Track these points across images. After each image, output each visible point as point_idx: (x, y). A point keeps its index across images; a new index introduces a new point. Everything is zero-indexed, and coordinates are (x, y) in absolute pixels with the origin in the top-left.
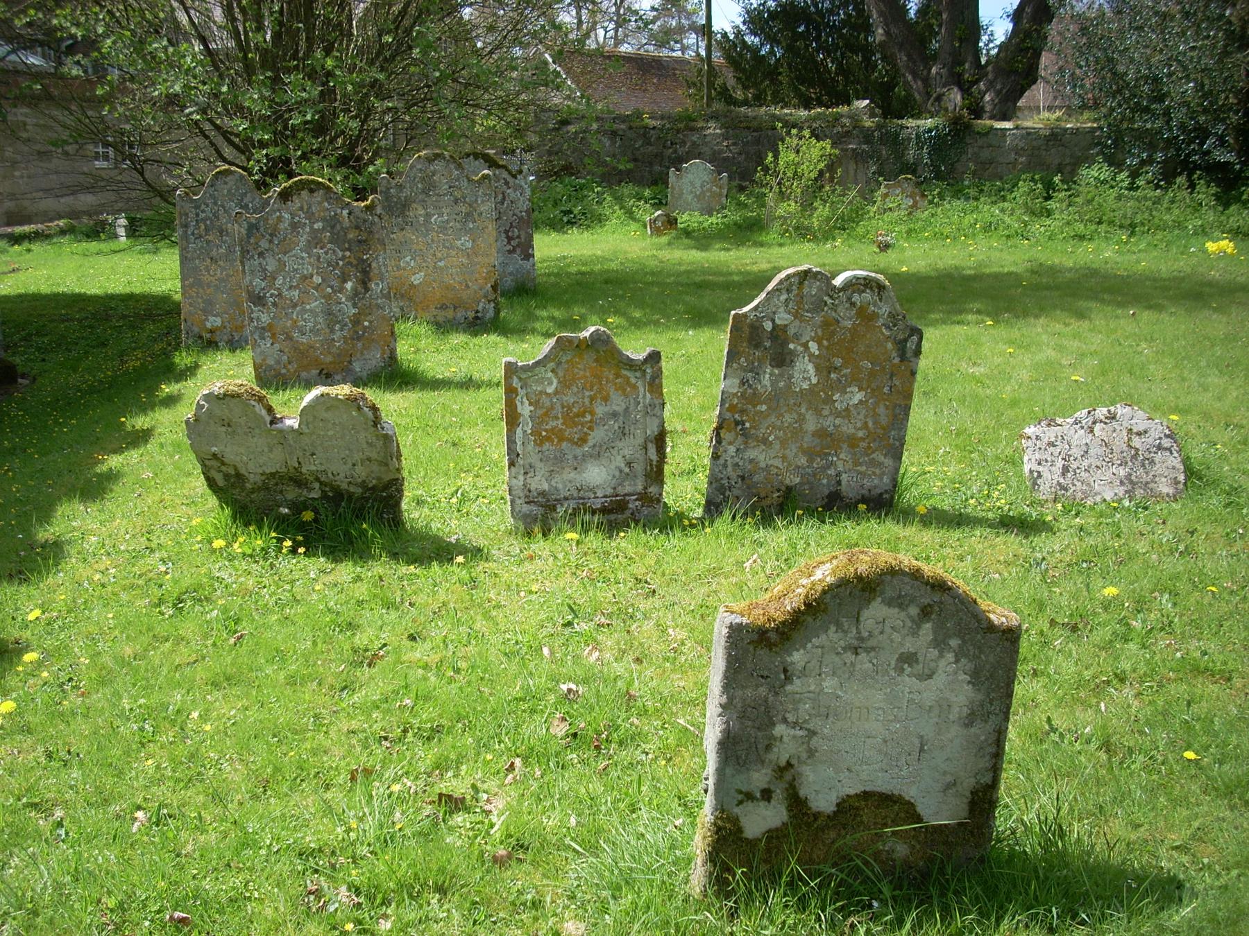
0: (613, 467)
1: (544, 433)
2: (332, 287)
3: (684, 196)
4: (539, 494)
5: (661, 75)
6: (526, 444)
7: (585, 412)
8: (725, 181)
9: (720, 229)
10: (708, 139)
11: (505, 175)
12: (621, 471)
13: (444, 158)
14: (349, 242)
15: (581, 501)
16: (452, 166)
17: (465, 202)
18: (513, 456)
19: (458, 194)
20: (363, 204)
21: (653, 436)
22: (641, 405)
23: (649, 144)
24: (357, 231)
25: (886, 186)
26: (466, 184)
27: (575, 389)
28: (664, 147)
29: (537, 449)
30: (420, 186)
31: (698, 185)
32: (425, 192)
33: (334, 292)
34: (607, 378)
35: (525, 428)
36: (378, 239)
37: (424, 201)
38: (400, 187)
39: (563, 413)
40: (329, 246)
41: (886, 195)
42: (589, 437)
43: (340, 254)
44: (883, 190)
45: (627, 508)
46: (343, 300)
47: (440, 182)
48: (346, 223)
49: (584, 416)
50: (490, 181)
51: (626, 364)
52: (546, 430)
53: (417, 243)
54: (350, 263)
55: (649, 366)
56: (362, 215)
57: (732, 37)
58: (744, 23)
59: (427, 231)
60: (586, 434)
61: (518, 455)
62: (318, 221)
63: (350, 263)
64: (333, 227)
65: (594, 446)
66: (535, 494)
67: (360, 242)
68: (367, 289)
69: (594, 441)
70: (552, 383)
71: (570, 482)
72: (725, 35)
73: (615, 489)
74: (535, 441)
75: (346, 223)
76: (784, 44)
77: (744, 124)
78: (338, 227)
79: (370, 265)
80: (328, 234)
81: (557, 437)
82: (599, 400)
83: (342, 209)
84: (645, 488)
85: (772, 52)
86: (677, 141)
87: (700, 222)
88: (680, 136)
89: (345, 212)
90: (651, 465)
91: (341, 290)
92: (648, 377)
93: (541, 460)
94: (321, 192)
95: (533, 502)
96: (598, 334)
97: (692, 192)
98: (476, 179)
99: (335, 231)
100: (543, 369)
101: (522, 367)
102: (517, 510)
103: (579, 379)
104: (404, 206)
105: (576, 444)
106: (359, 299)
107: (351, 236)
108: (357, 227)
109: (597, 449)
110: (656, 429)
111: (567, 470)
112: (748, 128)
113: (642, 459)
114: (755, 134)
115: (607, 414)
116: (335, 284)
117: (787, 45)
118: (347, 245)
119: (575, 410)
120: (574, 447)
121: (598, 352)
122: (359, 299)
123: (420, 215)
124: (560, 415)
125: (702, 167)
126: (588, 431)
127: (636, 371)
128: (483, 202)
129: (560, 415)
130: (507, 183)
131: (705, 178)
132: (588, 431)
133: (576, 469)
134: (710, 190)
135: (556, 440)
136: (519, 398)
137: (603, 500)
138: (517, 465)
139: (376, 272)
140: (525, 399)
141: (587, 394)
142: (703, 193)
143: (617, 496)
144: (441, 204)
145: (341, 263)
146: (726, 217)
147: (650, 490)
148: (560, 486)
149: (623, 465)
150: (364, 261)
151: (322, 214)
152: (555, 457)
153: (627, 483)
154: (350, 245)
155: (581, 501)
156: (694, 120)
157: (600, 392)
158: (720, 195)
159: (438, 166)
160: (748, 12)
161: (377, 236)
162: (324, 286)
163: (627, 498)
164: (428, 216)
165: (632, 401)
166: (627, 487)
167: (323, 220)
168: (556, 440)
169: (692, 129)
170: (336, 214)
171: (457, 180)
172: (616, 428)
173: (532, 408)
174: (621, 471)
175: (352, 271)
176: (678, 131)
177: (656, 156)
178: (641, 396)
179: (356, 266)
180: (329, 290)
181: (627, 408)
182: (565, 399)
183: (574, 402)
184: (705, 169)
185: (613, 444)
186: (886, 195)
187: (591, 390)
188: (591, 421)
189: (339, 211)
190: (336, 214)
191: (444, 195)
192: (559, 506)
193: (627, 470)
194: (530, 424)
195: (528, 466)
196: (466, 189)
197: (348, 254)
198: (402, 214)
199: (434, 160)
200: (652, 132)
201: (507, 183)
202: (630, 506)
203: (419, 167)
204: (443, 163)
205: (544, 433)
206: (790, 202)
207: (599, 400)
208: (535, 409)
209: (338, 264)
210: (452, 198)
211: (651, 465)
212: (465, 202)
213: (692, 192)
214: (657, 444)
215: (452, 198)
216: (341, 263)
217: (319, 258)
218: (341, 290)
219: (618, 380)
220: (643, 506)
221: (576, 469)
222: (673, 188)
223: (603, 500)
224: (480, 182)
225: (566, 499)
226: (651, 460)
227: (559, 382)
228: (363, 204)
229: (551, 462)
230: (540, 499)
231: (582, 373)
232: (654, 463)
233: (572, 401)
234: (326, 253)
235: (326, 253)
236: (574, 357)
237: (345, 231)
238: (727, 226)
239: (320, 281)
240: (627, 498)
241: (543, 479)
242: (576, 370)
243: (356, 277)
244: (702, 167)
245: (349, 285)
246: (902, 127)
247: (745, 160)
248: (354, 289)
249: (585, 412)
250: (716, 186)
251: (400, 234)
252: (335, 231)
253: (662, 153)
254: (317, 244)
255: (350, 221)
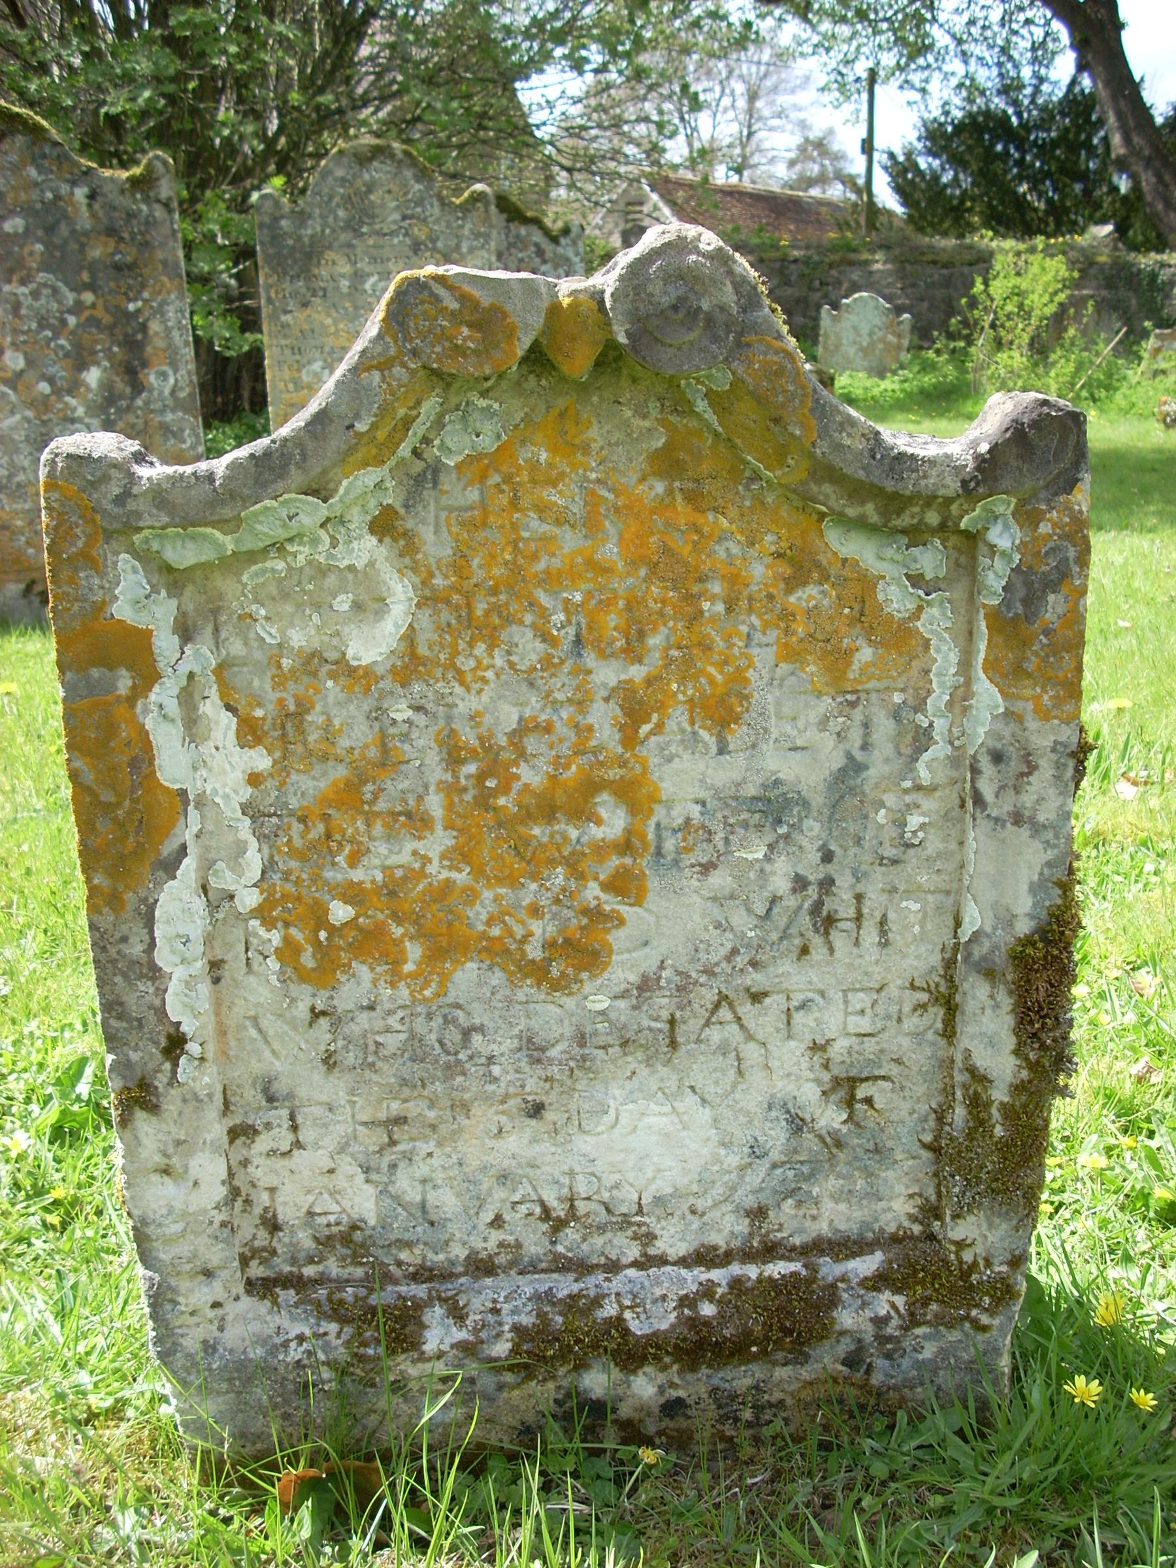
0: (752, 1098)
1: (340, 912)
2: (51, 380)
3: (843, 348)
4: (326, 1242)
5: (802, 221)
6: (235, 967)
7: (591, 787)
8: (906, 327)
9: (898, 399)
10: (876, 277)
11: (537, 236)
12: (798, 1124)
13: (392, 156)
14: (92, 267)
15: (565, 1285)
16: (409, 174)
17: (434, 249)
18: (143, 1055)
19: (420, 233)
20: (124, 175)
21: (1004, 939)
22: (939, 750)
23: (788, 283)
24: (112, 243)
25: (1157, 336)
26: (436, 211)
27: (530, 649)
28: (810, 289)
29: (305, 998)
30: (341, 213)
31: (865, 331)
32: (352, 226)
33: (57, 392)
34: (734, 580)
35: (224, 880)
36: (165, 263)
37: (350, 245)
38: (302, 217)
39: (451, 790)
40: (42, 277)
41: (1157, 351)
42: (618, 938)
43: (70, 298)
44: (1151, 343)
45: (822, 1330)
46: (81, 411)
47: (383, 206)
48: (84, 219)
49: (583, 814)
50: (487, 205)
51: (858, 491)
52: (352, 894)
53: (336, 334)
54: (94, 322)
55: (1004, 505)
56: (125, 202)
57: (901, 159)
58: (919, 139)
59: (356, 308)
60: (596, 915)
61: (175, 1044)
62: (12, 213)
63: (94, 322)
64: (51, 229)
65: (646, 986)
66: (305, 1240)
67: (118, 267)
68: (138, 387)
69: (647, 960)
70: (381, 604)
71: (504, 1178)
72: (892, 156)
73: (758, 1214)
74: (288, 952)
75: (84, 219)
76: (975, 167)
77: (929, 257)
78: (64, 229)
79: (144, 328)
80: (39, 247)
81: (421, 934)
82: (678, 718)
83: (74, 183)
84: (931, 1211)
85: (956, 181)
86: (830, 280)
87: (866, 389)
88: (834, 272)
89: (80, 193)
90: (977, 1104)
91: (74, 387)
92: (995, 577)
93: (330, 1062)
94: (20, 140)
95: (295, 1282)
96: (680, 275)
97: (855, 343)
98: (458, 201)
99: (57, 240)
100: (311, 512)
101: (160, 495)
102: (191, 1343)
103: (549, 580)
104: (309, 256)
105: (538, 972)
106: (120, 411)
107: (96, 253)
108: (111, 232)
109: (663, 1003)
110: (1023, 905)
111: (485, 1117)
112: (934, 263)
113: (920, 1057)
114: (944, 271)
115: (731, 799)
116: (60, 371)
117: (980, 170)
118: (85, 277)
119: (530, 776)
120: (527, 990)
121: (681, 405)
122: (120, 411)
123: (343, 276)
124: (435, 804)
125: (872, 304)
126: (610, 903)
127: (916, 536)
128: (471, 250)
129: (435, 804)
130: (540, 253)
131: (877, 321)
132: (610, 903)
133: (536, 1110)
134: (882, 340)
135: (414, 952)
136: (164, 694)
137: (694, 1277)
138: (171, 1103)
139: (161, 344)
140: (211, 708)
141: (607, 674)
142: (872, 344)
143: (770, 1251)
144: (386, 252)
145: (72, 320)
146: (905, 381)
147: (959, 1231)
148: (446, 1201)
149: (809, 1093)
150: (130, 316)
151: (23, 196)
152: (415, 1050)
153: (825, 1186)
154: (93, 276)
155: (565, 1285)
156: (855, 251)
157: (686, 669)
158: (899, 348)
159: (378, 172)
160: (925, 126)
161: (160, 255)
162: (30, 376)
163: (830, 1269)
164: (358, 277)
165: (884, 727)
166: (828, 1205)
167: (27, 210)
168: (414, 952)
169: (851, 263)
170: (58, 198)
171: (420, 202)
172: (781, 884)
173: (261, 760)
174: (798, 1124)
175: (102, 342)
176: (831, 266)
177: (798, 301)
178: (939, 698)
179: (111, 329)
180: (44, 387)
181: (853, 768)
182: (466, 703)
183: (525, 728)
184: (877, 308)
185: (755, 980)
186: (1157, 351)
187: (633, 653)
188: (626, 846)
189: (64, 189)
190: (58, 198)
191: (392, 234)
192: (435, 1315)
193: (832, 1118)
194: (254, 861)
195: (252, 1095)
196: (437, 221)
197: (88, 297)
198: (305, 272)
199: (370, 160)
200: (793, 267)
201: (540, 253)
202: (846, 1318)
203: (340, 173)
204: (389, 167)
205: (340, 912)
206: (1012, 353)
207: (678, 718)
208: (282, 767)
209: (64, 322)
210: (408, 241)
211: (977, 1104)
212: (434, 249)
213: (855, 343)
214: (1022, 992)
215: (408, 241)
216: (72, 320)
217: (16, 307)
218: (74, 387)
219: (808, 595)
220: (912, 1320)
221: (536, 1110)
222: (826, 335)
223: (694, 1277)
224: (466, 208)
225: (482, 1267)
226: (978, 1077)
227: (428, 599)
228: (124, 175)
229: (388, 1073)
230: (333, 1267)
231: (570, 541)
232: (1000, 1094)
233: (509, 717)
234: (35, 295)
235: (35, 295)
236: (521, 434)
237: (82, 239)
238: (909, 395)
239: (21, 363)
240: (830, 1269)
241: (348, 1167)
242: (535, 526)
243: (110, 357)
244: (872, 304)
245: (93, 376)
246: (1163, 265)
247: (929, 309)
248: (106, 385)
249: (591, 787)
250: (893, 333)
251: (301, 315)
252: (57, 240)
253: (806, 298)
254: (11, 271)
255: (94, 215)
